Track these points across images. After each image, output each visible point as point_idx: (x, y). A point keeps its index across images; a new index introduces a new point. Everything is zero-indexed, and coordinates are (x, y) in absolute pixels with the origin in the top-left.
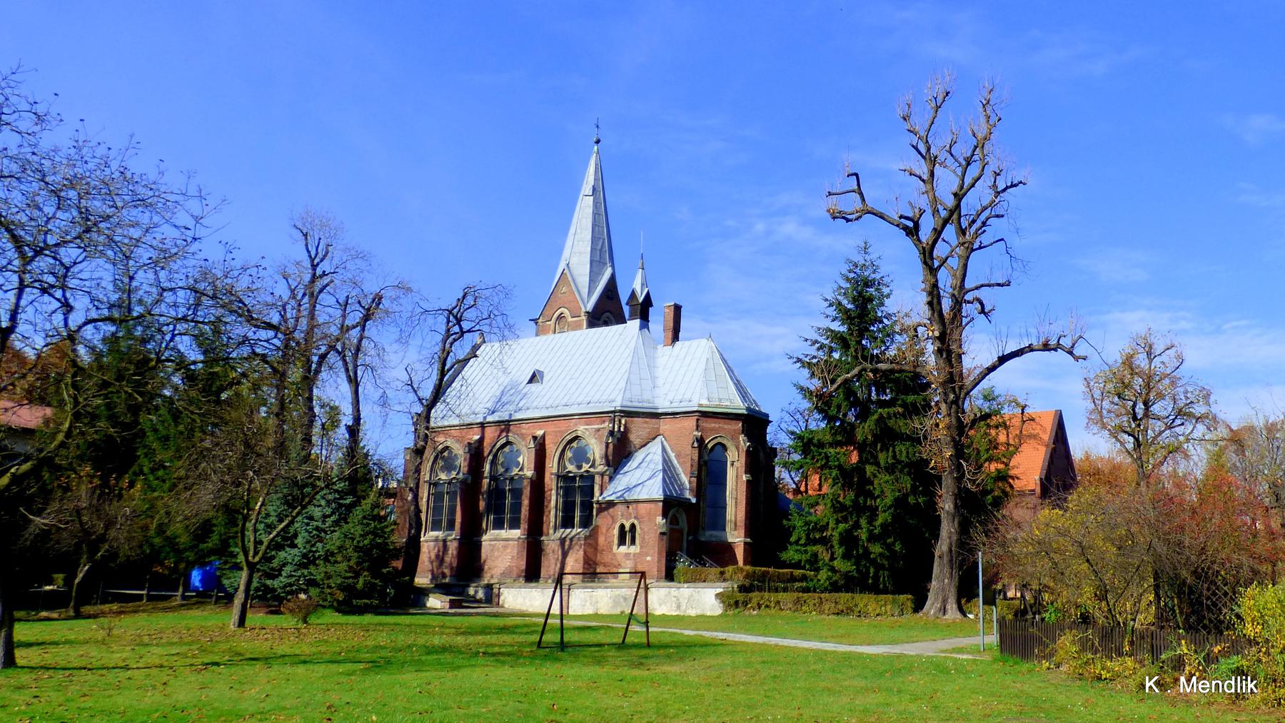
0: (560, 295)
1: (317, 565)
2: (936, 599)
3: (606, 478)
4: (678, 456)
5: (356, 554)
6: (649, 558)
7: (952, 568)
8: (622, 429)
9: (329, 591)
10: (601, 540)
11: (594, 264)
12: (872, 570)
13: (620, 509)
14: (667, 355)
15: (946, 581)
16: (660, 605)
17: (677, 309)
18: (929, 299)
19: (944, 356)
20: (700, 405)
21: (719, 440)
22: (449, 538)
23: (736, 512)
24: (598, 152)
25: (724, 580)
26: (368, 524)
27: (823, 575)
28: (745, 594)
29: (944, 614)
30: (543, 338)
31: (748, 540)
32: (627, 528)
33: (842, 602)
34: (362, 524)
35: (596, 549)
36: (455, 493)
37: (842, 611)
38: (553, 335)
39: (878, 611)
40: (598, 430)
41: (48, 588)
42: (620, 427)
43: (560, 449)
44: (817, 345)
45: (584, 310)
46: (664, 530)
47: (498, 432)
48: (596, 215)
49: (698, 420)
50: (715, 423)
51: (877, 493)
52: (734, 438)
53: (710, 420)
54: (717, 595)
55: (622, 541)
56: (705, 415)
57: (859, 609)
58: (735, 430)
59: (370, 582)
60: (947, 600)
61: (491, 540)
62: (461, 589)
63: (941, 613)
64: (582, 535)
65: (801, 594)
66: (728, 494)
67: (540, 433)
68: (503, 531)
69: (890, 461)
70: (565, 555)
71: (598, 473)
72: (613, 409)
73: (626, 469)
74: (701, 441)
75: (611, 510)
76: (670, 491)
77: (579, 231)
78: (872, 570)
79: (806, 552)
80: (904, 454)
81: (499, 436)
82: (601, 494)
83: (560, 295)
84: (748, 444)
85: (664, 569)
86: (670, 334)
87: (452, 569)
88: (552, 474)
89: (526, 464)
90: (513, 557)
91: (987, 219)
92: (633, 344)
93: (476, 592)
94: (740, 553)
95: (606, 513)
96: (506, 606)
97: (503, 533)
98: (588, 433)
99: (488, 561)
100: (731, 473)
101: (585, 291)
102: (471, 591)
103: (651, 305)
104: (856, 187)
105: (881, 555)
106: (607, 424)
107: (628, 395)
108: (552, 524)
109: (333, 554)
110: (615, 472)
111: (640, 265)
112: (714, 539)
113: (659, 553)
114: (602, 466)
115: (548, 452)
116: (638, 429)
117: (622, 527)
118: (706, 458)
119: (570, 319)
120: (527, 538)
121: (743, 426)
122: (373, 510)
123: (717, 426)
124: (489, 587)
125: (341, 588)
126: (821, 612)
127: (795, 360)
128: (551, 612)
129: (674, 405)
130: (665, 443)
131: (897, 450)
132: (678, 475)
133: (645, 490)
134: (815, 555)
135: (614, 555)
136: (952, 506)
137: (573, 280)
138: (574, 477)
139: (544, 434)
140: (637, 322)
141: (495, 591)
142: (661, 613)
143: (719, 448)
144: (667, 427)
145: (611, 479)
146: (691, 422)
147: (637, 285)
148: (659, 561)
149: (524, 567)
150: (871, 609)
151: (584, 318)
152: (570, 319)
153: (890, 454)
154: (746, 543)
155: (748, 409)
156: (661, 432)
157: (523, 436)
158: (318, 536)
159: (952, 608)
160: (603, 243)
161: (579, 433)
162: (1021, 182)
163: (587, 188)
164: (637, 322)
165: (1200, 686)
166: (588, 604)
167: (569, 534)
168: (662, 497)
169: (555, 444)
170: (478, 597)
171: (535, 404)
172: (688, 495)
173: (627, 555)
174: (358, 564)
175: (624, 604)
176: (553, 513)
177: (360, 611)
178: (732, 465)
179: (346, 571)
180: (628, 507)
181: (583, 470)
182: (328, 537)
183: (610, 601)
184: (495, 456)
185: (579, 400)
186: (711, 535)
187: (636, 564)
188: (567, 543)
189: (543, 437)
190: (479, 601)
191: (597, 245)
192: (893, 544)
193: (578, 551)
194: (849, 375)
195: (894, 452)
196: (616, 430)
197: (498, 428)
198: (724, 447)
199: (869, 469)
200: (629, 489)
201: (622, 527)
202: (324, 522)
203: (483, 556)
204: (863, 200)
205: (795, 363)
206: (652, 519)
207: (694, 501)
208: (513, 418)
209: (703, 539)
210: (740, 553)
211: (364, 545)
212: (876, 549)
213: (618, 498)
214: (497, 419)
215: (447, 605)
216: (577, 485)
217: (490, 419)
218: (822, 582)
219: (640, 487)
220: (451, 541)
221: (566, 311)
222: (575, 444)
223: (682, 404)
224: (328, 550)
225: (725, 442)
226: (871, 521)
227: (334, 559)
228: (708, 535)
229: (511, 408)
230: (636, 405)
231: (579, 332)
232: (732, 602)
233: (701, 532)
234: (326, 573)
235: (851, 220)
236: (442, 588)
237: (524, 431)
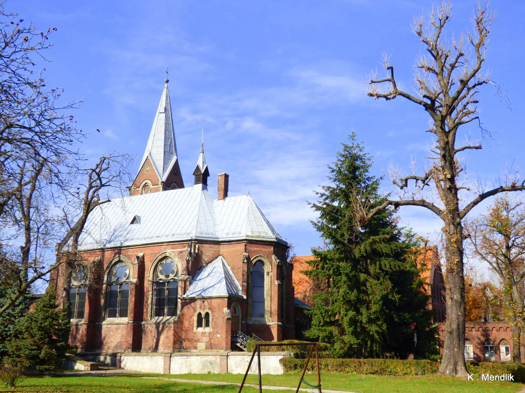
0: (145, 172)
1: (10, 341)
2: (449, 363)
3: (188, 283)
4: (232, 269)
5: (40, 333)
6: (218, 336)
7: (459, 341)
8: (196, 251)
9: (17, 360)
10: (186, 324)
11: (166, 153)
12: (369, 343)
13: (199, 303)
14: (220, 205)
15: (456, 349)
16: (237, 367)
17: (226, 177)
18: (443, 153)
19: (453, 192)
20: (247, 236)
21: (259, 258)
22: (80, 323)
23: (271, 305)
24: (167, 88)
25: (282, 350)
26: (47, 311)
27: (337, 346)
28: (302, 360)
29: (456, 374)
30: (134, 198)
31: (280, 323)
32: (203, 315)
33: (377, 364)
34: (44, 311)
35: (182, 329)
36: (84, 294)
37: (377, 371)
38: (141, 196)
39: (405, 372)
40: (181, 252)
41: (415, 339)
42: (195, 250)
43: (154, 264)
44: (324, 197)
45: (160, 181)
46: (230, 316)
47: (113, 255)
48: (167, 124)
49: (246, 245)
50: (257, 247)
51: (369, 292)
52: (269, 257)
53: (253, 245)
54: (280, 360)
55: (199, 325)
56: (250, 242)
57: (390, 370)
58: (269, 252)
59: (49, 353)
60: (457, 363)
61: (107, 324)
62: (93, 357)
63: (454, 373)
64: (172, 320)
65: (344, 360)
66: (265, 296)
67: (141, 254)
68: (116, 318)
69: (378, 271)
70: (159, 334)
71: (181, 280)
72: (190, 238)
73: (199, 277)
74: (248, 258)
75: (192, 304)
76: (231, 291)
77: (156, 134)
78: (369, 343)
79: (325, 331)
80: (388, 266)
81: (114, 257)
82: (185, 293)
83: (145, 172)
84: (278, 261)
85: (230, 343)
86: (222, 193)
87: (82, 343)
88: (149, 281)
89: (131, 275)
90: (122, 335)
91: (468, 103)
92: (198, 199)
93: (105, 359)
94: (275, 332)
95: (189, 306)
96: (126, 368)
97: (118, 320)
98: (173, 254)
99: (107, 338)
100: (267, 280)
101: (161, 169)
102: (102, 358)
103: (208, 175)
104: (390, 77)
105: (377, 332)
106: (186, 248)
107: (199, 230)
108: (149, 314)
109: (21, 333)
110: (192, 279)
111: (201, 150)
112: (257, 323)
113: (227, 332)
114: (183, 276)
115: (146, 266)
116: (207, 251)
117: (200, 314)
118: (252, 270)
119: (151, 187)
120: (133, 323)
121: (274, 250)
122: (50, 301)
123: (258, 249)
124: (114, 356)
125: (28, 358)
126: (361, 373)
127: (312, 205)
128: (262, 374)
129: (229, 236)
130: (224, 260)
131: (382, 263)
132: (233, 281)
133: (215, 291)
134: (331, 333)
135: (195, 333)
136: (459, 297)
137: (154, 163)
138: (163, 284)
139: (144, 255)
140: (200, 186)
141: (118, 358)
142: (237, 373)
143: (259, 263)
144: (225, 250)
145: (191, 283)
146: (241, 247)
147: (200, 163)
148: (227, 337)
149: (131, 342)
150: (399, 370)
151: (160, 186)
152: (151, 187)
153: (378, 266)
154: (278, 325)
155: (277, 238)
156: (221, 253)
157: (129, 257)
158: (9, 320)
159: (461, 369)
160: (171, 141)
161: (167, 254)
162: (484, 82)
163: (161, 107)
164: (200, 186)
165: (490, 378)
166: (184, 366)
167: (162, 319)
168: (227, 295)
169: (151, 261)
170: (106, 362)
171: (136, 236)
172: (240, 293)
173: (203, 333)
174: (40, 339)
175: (210, 367)
176: (150, 306)
177: (41, 374)
178: (268, 274)
179: (31, 345)
180: (204, 302)
181: (170, 278)
182: (17, 320)
183: (201, 364)
184: (110, 271)
185: (167, 233)
186: (256, 320)
187: (210, 339)
188: (161, 326)
189: (143, 257)
190: (107, 365)
191: (168, 142)
192: (381, 325)
193: (168, 331)
194: (381, 207)
195: (380, 265)
196: (192, 251)
197: (113, 252)
198: (262, 263)
199: (363, 276)
200: (204, 290)
201: (200, 314)
202: (13, 310)
203: (103, 335)
204: (395, 86)
205: (312, 207)
206: (221, 310)
207: (245, 297)
208: (123, 245)
209: (251, 323)
210: (275, 332)
211: (45, 326)
212: (373, 329)
213: (198, 295)
214: (112, 246)
215: (89, 369)
216: (166, 288)
217: (108, 246)
218: (337, 351)
219: (211, 289)
220: (81, 325)
221: (149, 183)
222: (164, 262)
223: (235, 236)
224: (17, 330)
225: (263, 259)
226: (368, 308)
227: (21, 336)
228: (253, 320)
229: (121, 239)
230: (205, 235)
231: (157, 193)
232: (292, 365)
234: (17, 346)
235: (389, 99)
236: (84, 357)
237: (130, 253)
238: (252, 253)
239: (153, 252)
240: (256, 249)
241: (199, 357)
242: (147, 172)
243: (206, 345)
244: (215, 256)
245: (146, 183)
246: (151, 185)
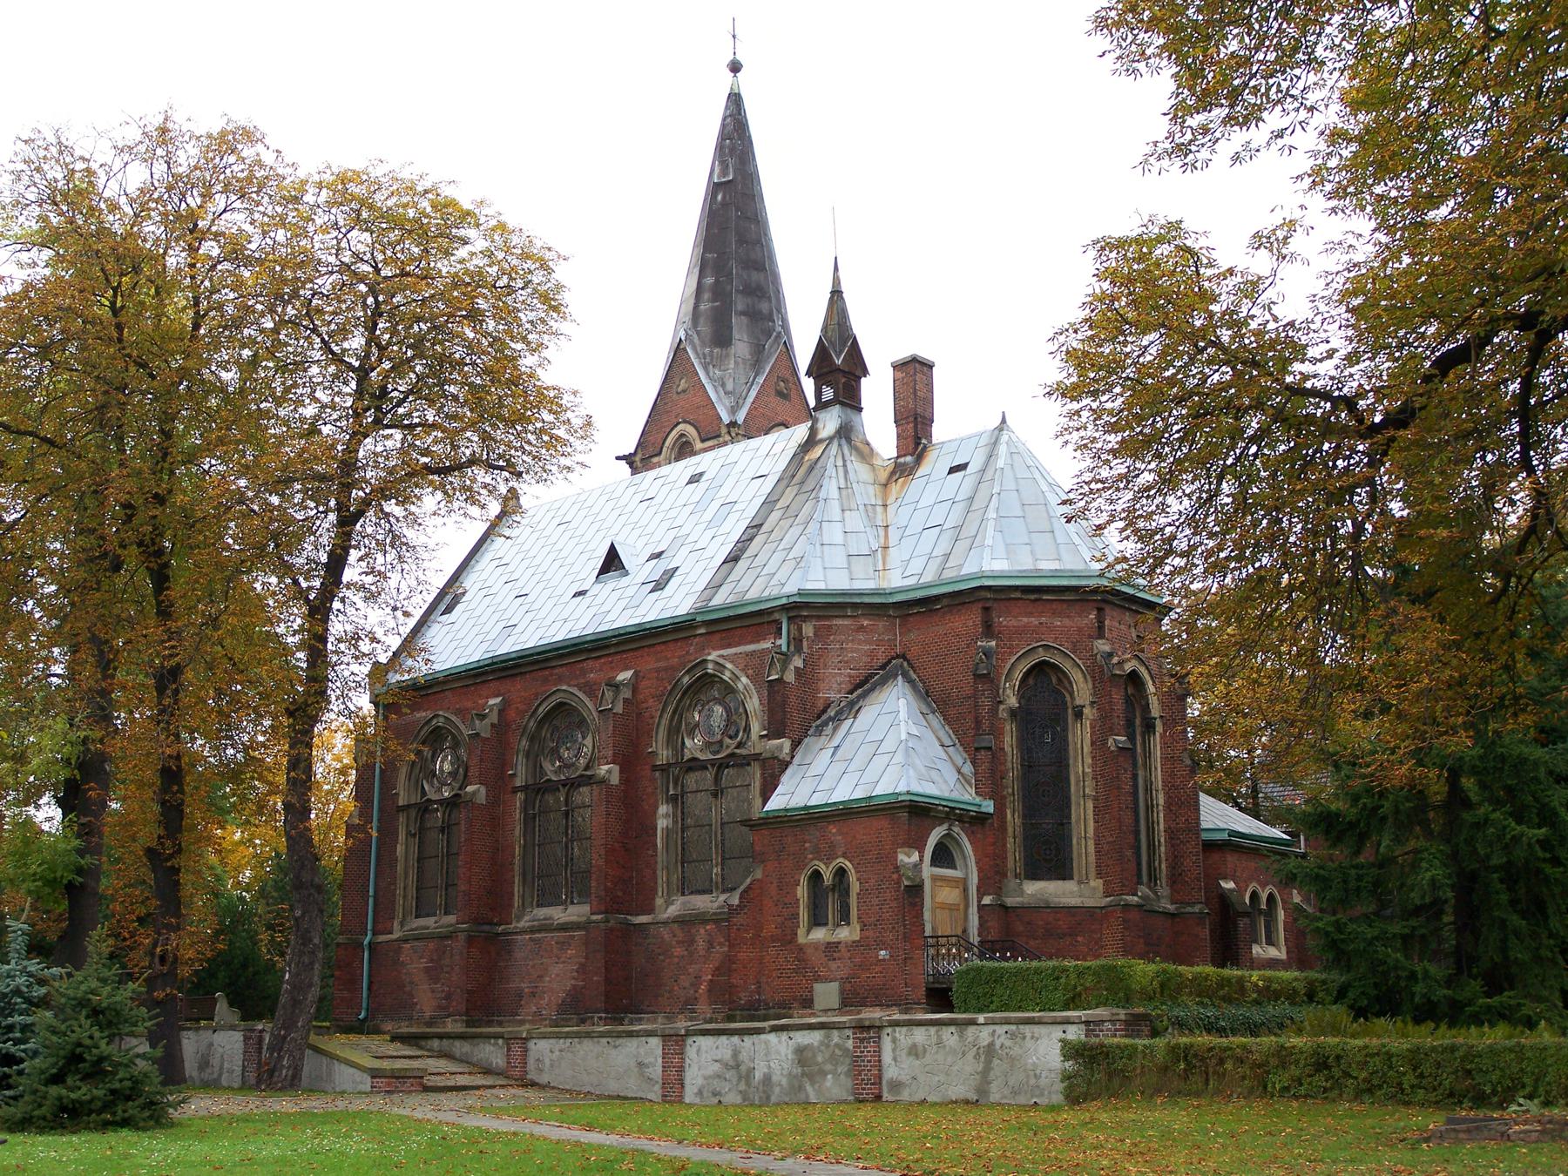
21: (1042, 655)
50: (1030, 614)
58: (1080, 630)
66: (1073, 789)
123: (1034, 621)
135: (801, 948)
173: (831, 948)
201: (816, 876)
233: (1012, 883)
238: (1010, 639)
239: (662, 664)
240: (1025, 620)
242: (682, 396)
243: (842, 991)
245: (682, 435)
246: (698, 441)
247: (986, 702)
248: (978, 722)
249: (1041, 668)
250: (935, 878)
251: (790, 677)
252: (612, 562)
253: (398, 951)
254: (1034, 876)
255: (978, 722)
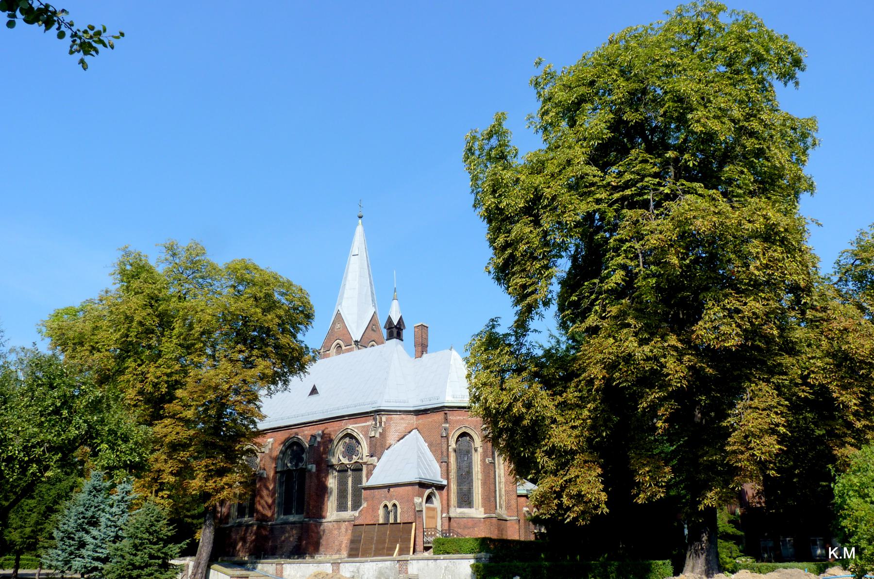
21: (464, 430)
50: (460, 416)
123: (461, 418)
129: (424, 403)
225: (472, 433)
241: (374, 563)
244: (407, 431)
247: (445, 446)
248: (442, 453)
249: (464, 434)
250: (428, 508)
251: (377, 435)
252: (314, 391)
253: (231, 531)
254: (460, 506)
255: (442, 453)
